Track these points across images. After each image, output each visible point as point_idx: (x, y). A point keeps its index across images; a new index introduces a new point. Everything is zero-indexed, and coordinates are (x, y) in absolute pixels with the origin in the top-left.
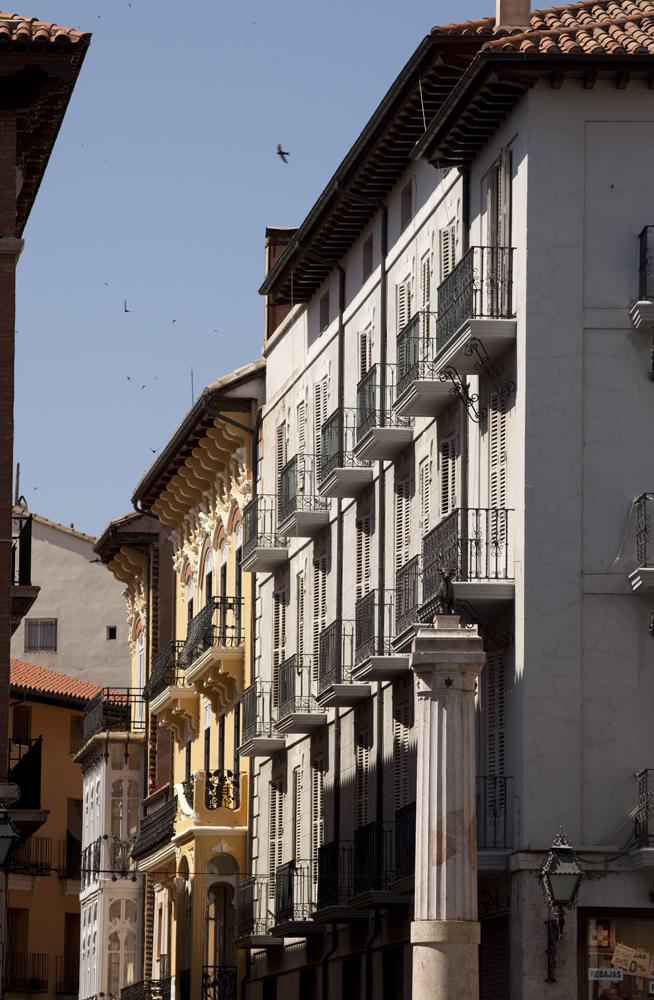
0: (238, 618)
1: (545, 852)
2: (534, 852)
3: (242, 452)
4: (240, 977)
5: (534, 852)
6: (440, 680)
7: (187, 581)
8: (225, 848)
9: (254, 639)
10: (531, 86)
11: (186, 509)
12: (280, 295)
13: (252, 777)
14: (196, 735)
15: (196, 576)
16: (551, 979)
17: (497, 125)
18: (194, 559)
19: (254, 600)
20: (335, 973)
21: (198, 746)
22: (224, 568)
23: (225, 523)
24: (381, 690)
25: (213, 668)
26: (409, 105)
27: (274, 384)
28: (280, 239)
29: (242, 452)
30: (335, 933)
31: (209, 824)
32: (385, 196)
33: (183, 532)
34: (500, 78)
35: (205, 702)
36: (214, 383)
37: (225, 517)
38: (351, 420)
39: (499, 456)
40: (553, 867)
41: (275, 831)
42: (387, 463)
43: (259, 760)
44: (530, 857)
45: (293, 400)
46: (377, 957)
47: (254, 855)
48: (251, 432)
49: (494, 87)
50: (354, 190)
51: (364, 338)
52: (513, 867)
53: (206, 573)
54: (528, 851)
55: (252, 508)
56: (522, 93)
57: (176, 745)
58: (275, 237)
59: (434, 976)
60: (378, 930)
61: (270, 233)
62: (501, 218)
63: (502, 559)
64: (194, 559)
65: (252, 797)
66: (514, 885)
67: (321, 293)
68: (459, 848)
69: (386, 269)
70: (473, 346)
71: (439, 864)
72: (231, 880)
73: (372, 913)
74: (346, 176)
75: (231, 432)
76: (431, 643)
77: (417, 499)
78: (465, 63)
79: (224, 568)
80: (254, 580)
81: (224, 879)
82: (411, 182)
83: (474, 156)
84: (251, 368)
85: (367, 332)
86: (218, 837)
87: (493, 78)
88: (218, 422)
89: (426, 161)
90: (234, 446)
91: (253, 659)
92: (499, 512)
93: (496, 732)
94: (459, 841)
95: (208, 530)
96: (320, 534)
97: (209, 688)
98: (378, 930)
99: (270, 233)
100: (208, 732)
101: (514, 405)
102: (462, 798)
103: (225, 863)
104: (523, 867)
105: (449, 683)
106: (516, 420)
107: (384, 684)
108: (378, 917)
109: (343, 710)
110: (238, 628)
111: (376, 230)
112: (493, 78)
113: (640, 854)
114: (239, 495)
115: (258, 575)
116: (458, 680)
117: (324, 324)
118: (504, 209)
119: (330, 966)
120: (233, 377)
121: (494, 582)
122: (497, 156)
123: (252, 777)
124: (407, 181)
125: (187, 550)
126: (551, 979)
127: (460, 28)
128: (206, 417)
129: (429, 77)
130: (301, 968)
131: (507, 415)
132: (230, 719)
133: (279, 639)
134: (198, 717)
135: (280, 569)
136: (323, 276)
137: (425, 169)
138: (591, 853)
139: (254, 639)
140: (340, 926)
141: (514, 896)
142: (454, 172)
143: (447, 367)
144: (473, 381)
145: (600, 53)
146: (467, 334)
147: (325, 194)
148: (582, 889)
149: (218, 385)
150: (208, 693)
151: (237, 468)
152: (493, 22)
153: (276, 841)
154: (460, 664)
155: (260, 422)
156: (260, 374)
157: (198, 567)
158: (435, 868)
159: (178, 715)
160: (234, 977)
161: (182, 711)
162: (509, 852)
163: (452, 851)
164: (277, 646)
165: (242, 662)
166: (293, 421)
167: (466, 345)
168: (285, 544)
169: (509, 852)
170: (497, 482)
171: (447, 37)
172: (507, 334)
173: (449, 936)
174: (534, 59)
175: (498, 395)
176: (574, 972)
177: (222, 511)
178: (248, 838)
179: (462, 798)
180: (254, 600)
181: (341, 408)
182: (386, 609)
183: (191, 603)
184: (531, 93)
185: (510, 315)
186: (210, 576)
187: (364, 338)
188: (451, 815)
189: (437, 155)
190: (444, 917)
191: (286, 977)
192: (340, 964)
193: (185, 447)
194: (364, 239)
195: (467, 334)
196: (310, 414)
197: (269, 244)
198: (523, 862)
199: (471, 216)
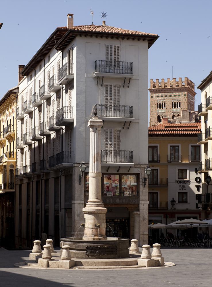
0: (14, 127)
1: (80, 164)
2: (77, 163)
3: (15, 101)
4: (15, 184)
5: (77, 163)
6: (95, 128)
7: (3, 122)
8: (12, 164)
9: (17, 131)
10: (77, 36)
11: (3, 110)
12: (23, 75)
13: (17, 153)
14: (5, 146)
15: (5, 121)
16: (80, 184)
17: (69, 43)
18: (5, 119)
19: (17, 124)
20: (34, 184)
21: (5, 148)
22: (11, 120)
23: (11, 112)
24: (44, 138)
25: (10, 135)
26: (53, 39)
27: (20, 90)
28: (21, 67)
29: (15, 101)
30: (34, 177)
31: (9, 160)
32: (44, 57)
33: (2, 114)
34: (72, 34)
35: (7, 141)
36: (11, 89)
37: (11, 112)
38: (38, 94)
39: (70, 97)
40: (82, 166)
41: (21, 161)
42: (45, 101)
43: (18, 150)
44: (77, 164)
45: (25, 92)
46: (43, 181)
47: (17, 165)
48: (16, 97)
49: (71, 36)
50: (40, 56)
51: (40, 81)
52: (74, 165)
53: (7, 120)
54: (76, 163)
55: (17, 109)
56: (75, 37)
57: (1, 148)
58: (20, 66)
59: (93, 183)
60: (43, 176)
61: (19, 65)
62: (71, 58)
63: (71, 115)
64: (5, 119)
65: (17, 156)
66: (74, 169)
67: (30, 74)
68: (98, 160)
69: (45, 69)
70: (67, 79)
71: (95, 162)
72: (13, 169)
73: (42, 174)
74: (38, 54)
75: (13, 97)
76: (93, 122)
77: (51, 106)
78: (64, 34)
79: (11, 120)
80: (17, 121)
81: (12, 169)
82: (50, 55)
83: (64, 49)
84: (16, 87)
85: (40, 80)
86: (11, 162)
87: (71, 34)
88: (11, 96)
89: (55, 50)
90: (13, 100)
91: (17, 134)
92: (70, 107)
93: (70, 144)
94: (98, 158)
95: (7, 113)
96: (30, 114)
97: (8, 139)
98: (43, 176)
99: (19, 65)
100: (7, 146)
101: (73, 88)
102: (99, 150)
103: (12, 166)
104: (76, 166)
105: (96, 129)
106: (74, 92)
107: (44, 137)
108: (43, 174)
109: (35, 141)
110: (14, 129)
111: (42, 63)
112: (71, 34)
113: (63, 164)
114: (14, 107)
115: (18, 120)
116: (98, 129)
117: (31, 79)
118: (71, 57)
119: (33, 182)
120: (13, 88)
121: (71, 119)
122: (69, 48)
123: (17, 153)
124: (49, 55)
125: (3, 117)
126: (80, 184)
127: (62, 28)
128: (8, 95)
129: (56, 36)
130: (27, 183)
131: (72, 90)
132: (12, 143)
133: (22, 130)
134: (5, 143)
135: (22, 119)
136: (31, 71)
137: (55, 50)
138: (87, 164)
139: (17, 131)
140: (35, 176)
141: (73, 171)
142: (60, 52)
143: (61, 83)
144: (64, 86)
145: (89, 31)
146: (66, 77)
147: (34, 57)
148: (86, 170)
149: (11, 90)
150: (8, 139)
151: (14, 103)
152: (67, 27)
153: (22, 163)
154: (99, 126)
155: (18, 96)
156: (18, 88)
157: (5, 120)
158: (94, 163)
159: (2, 143)
160: (14, 184)
161: (3, 142)
162: (72, 163)
163: (97, 160)
164: (22, 131)
165: (15, 134)
166: (25, 95)
167: (65, 79)
168: (23, 115)
169: (72, 163)
170: (70, 102)
171: (60, 29)
172: (72, 78)
173: (97, 175)
174: (78, 32)
175: (72, 88)
176: (84, 183)
177: (10, 110)
178: (16, 162)
179: (99, 150)
180: (17, 124)
181: (35, 93)
182: (45, 125)
183: (4, 125)
184: (77, 37)
185: (72, 74)
186: (8, 121)
187: (40, 81)
188: (97, 153)
189: (58, 48)
190: (95, 172)
191: (24, 184)
192: (35, 182)
193: (4, 100)
194: (40, 64)
195: (66, 77)
196: (29, 94)
197: (19, 67)
198: (76, 165)
199: (63, 58)
